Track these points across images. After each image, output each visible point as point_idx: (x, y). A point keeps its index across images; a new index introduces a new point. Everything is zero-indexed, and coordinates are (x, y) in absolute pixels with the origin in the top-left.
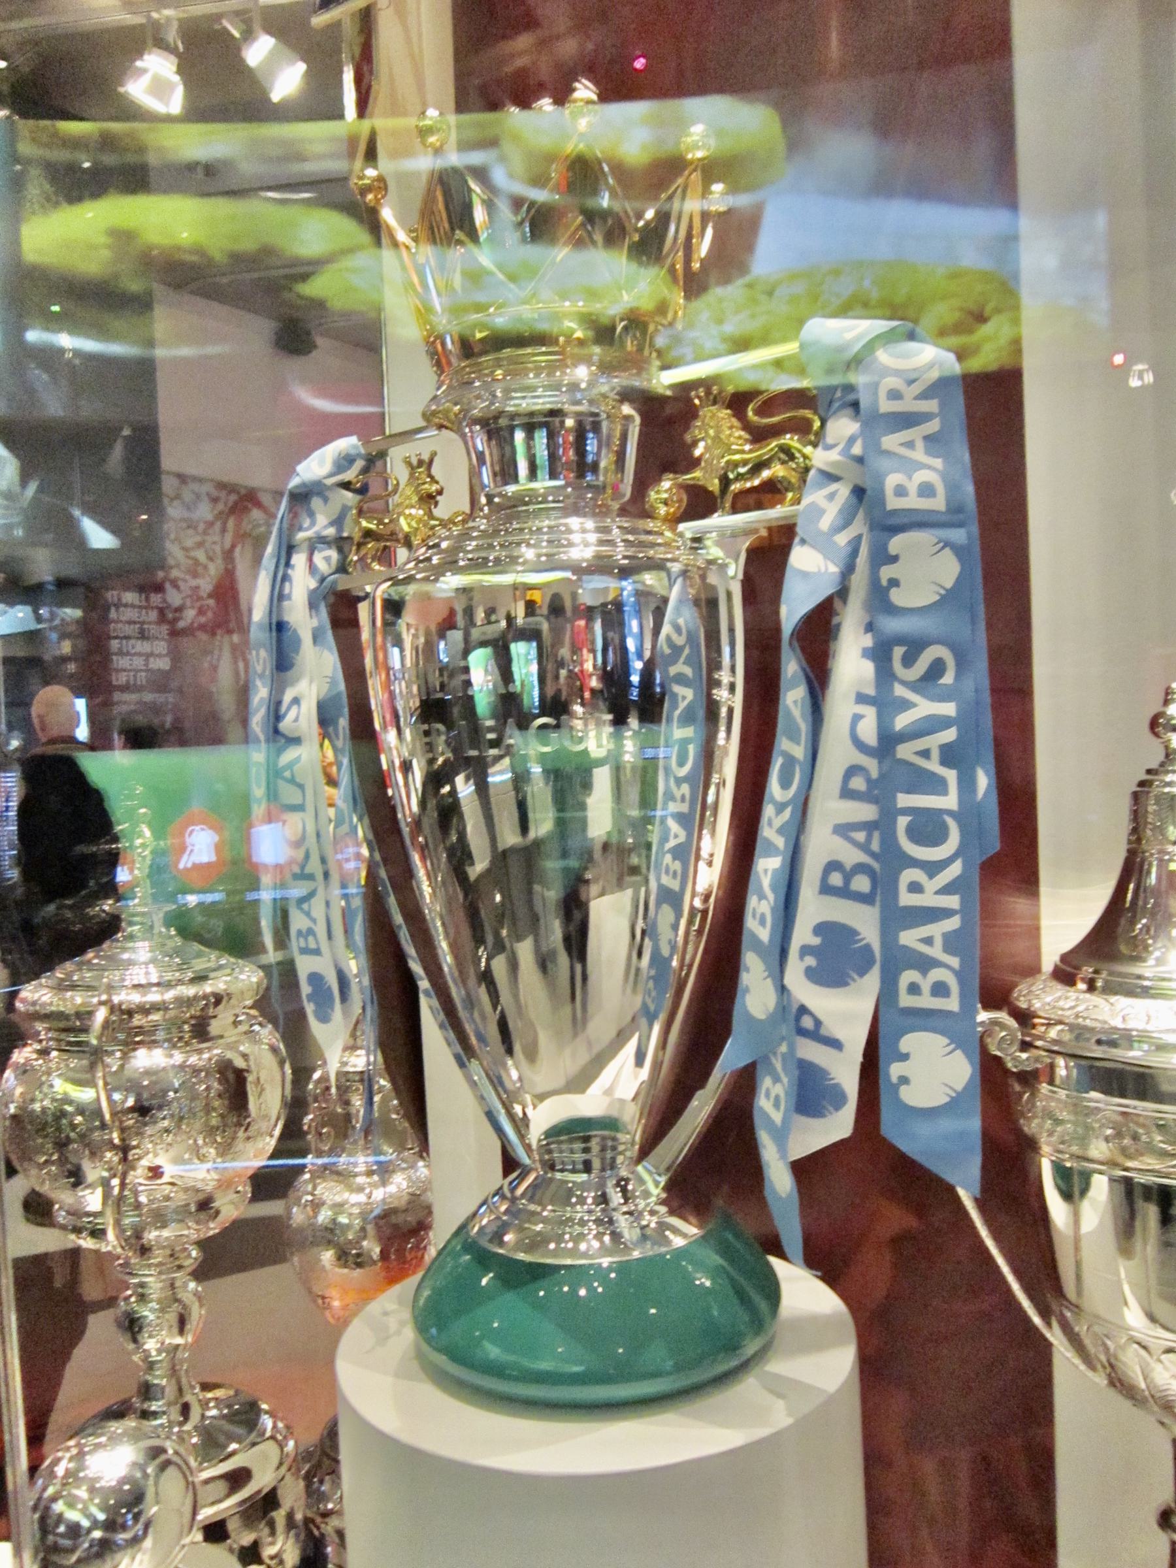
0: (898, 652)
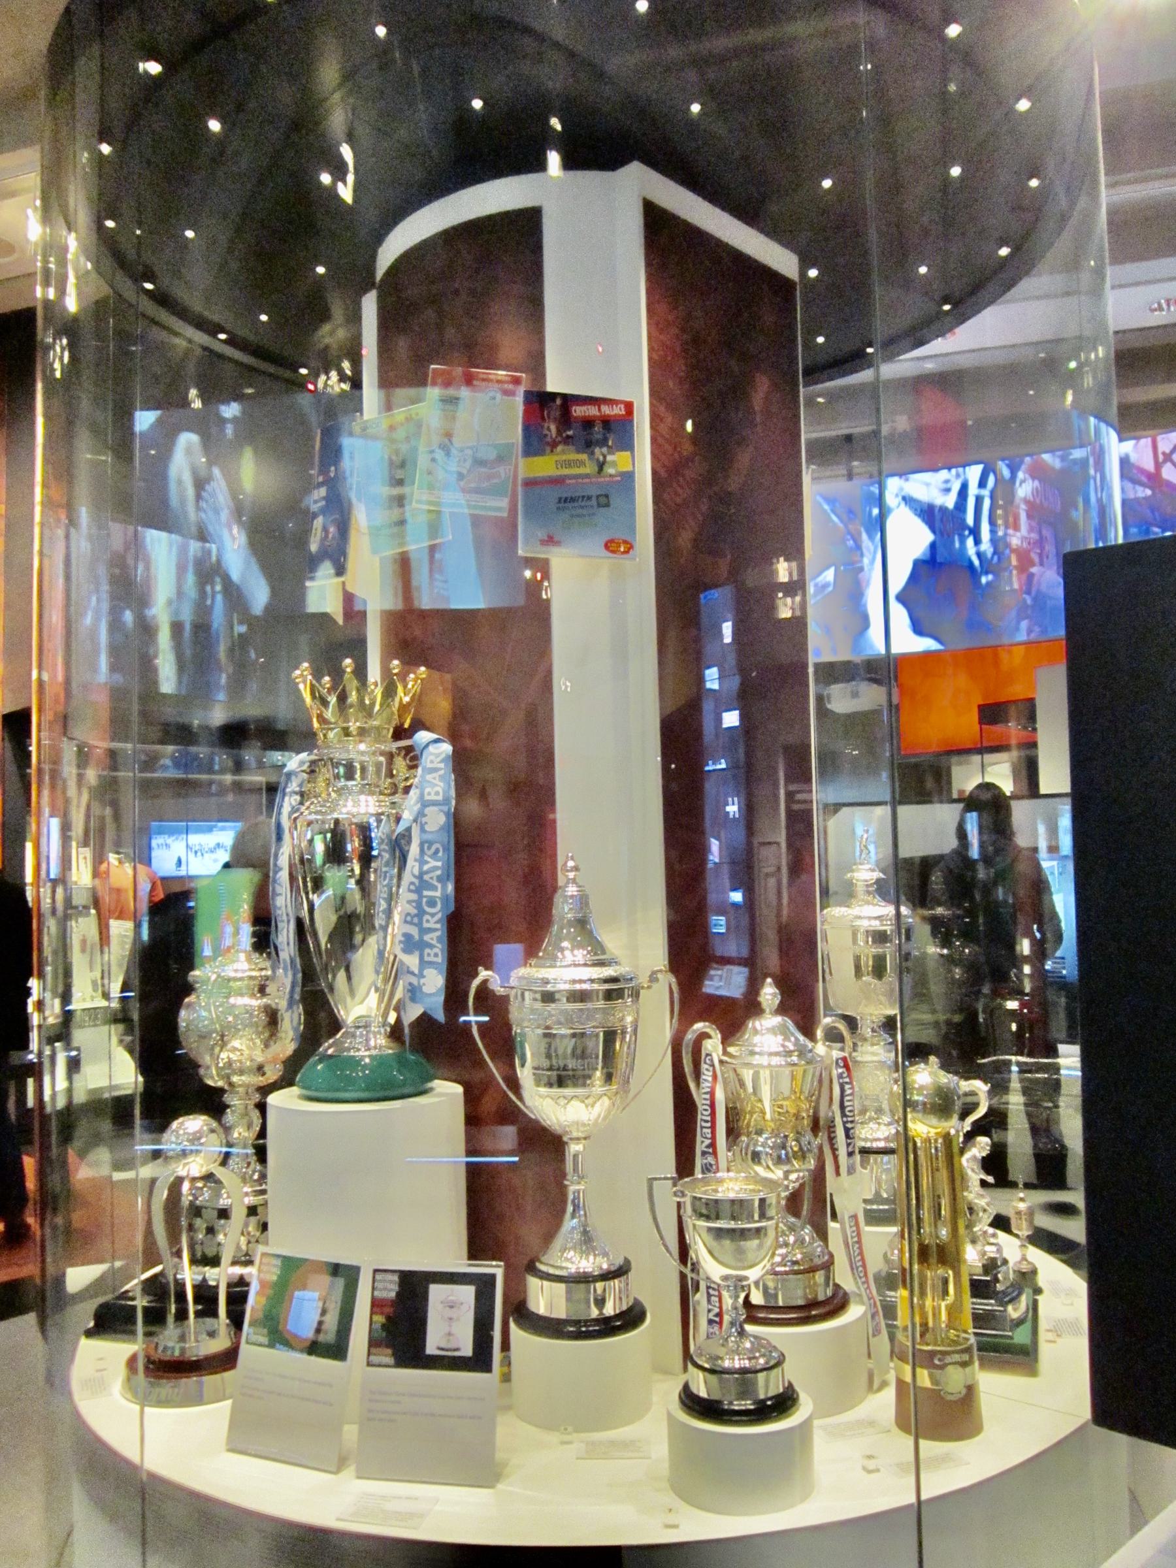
0: (426, 846)
